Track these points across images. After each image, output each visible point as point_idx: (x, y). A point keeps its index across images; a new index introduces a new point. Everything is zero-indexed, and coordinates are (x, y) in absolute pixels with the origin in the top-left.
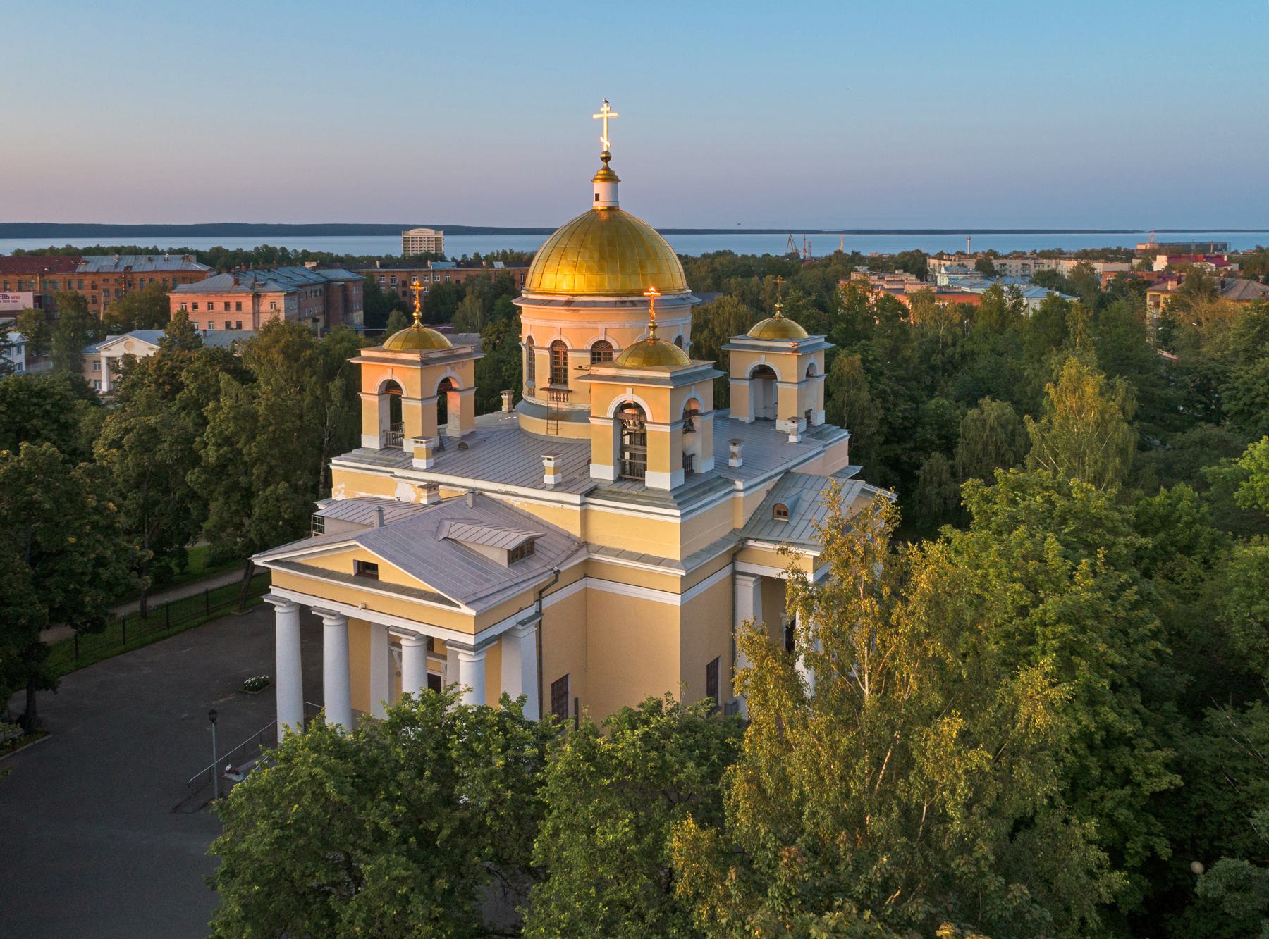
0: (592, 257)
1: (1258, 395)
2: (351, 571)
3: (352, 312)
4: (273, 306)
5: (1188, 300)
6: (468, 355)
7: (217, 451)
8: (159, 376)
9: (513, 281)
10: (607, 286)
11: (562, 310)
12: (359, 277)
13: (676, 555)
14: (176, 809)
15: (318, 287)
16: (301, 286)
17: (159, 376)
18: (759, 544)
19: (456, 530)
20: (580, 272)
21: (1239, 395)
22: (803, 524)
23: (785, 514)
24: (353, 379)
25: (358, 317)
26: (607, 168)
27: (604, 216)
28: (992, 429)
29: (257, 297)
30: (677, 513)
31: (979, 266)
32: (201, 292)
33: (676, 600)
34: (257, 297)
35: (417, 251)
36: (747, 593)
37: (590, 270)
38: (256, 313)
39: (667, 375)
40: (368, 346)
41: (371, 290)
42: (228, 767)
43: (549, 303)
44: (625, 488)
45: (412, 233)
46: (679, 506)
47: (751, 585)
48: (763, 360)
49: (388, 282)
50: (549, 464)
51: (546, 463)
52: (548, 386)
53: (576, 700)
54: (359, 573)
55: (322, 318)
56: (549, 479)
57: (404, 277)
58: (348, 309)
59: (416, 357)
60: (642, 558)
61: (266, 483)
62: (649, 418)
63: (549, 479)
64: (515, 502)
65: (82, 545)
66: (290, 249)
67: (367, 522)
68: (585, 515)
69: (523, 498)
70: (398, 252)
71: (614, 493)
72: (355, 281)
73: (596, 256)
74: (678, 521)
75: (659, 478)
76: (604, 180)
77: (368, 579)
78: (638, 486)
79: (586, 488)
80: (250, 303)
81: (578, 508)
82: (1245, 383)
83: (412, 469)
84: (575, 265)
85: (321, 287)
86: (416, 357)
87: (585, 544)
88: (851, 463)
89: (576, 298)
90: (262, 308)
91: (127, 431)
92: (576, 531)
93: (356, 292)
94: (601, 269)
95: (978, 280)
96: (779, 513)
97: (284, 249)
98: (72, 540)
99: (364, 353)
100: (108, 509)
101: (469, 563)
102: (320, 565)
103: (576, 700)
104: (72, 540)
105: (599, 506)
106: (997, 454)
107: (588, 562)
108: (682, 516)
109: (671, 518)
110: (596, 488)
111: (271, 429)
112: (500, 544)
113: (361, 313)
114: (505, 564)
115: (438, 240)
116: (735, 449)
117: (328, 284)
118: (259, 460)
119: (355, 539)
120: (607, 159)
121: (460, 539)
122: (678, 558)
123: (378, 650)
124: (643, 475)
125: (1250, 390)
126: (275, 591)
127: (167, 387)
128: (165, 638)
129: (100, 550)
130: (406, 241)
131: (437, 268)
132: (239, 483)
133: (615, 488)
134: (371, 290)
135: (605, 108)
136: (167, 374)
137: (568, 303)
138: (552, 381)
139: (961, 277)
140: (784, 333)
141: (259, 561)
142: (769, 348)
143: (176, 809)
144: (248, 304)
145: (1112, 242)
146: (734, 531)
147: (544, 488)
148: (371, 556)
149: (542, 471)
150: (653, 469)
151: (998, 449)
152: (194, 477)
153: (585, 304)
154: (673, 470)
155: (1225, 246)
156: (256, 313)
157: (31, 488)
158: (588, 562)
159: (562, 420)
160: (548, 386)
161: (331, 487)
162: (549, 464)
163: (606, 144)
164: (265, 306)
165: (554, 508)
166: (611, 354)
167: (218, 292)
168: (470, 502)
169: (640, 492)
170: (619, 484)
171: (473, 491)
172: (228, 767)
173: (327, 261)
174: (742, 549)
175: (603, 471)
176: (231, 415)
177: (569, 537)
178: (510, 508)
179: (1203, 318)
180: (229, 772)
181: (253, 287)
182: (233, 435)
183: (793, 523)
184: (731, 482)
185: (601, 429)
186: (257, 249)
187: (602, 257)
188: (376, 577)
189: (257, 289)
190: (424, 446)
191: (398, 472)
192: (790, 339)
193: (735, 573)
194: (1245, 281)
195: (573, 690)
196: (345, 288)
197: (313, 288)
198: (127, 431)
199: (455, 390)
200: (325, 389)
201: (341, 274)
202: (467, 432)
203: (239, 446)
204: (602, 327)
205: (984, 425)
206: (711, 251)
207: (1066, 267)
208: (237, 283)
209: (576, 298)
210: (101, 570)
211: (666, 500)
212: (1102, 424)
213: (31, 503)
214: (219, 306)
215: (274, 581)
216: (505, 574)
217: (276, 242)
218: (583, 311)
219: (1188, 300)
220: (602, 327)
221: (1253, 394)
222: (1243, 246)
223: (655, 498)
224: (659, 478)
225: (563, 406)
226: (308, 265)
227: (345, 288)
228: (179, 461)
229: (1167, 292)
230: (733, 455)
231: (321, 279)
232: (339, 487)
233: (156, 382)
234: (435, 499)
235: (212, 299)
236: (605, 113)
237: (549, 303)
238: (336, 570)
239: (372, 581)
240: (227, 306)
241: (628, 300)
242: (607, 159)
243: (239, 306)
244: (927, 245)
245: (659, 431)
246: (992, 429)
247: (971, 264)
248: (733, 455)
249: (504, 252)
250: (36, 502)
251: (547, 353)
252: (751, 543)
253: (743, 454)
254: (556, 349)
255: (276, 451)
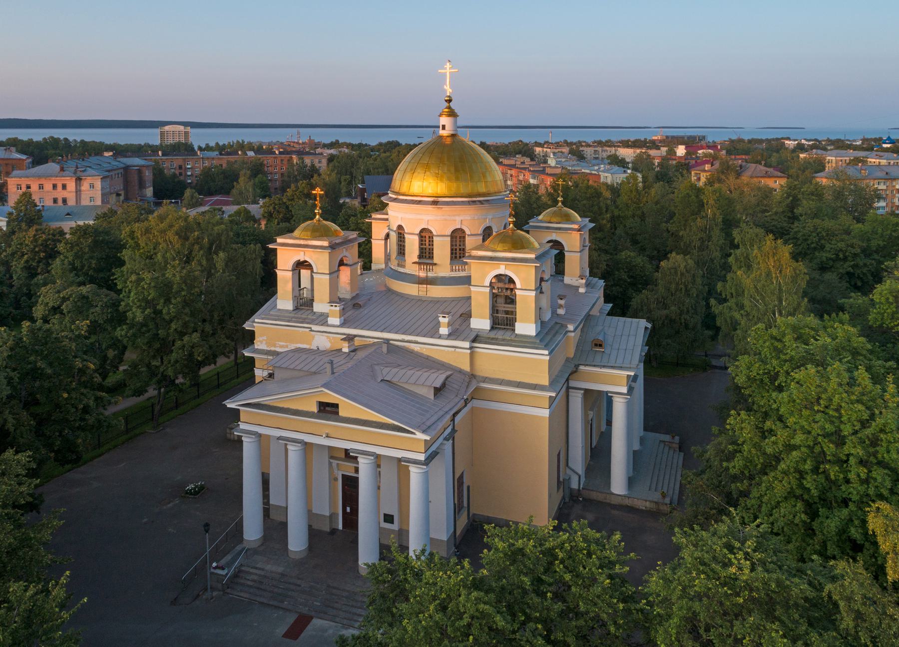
0: (449, 170)
1: (812, 243)
2: (315, 409)
3: (145, 188)
4: (92, 186)
5: (723, 177)
6: (355, 239)
7: (143, 312)
8: (35, 247)
9: (262, 164)
10: (462, 190)
11: (430, 208)
12: (150, 163)
13: (545, 382)
14: (174, 602)
15: (120, 171)
16: (109, 171)
17: (35, 247)
18: (587, 368)
19: (390, 373)
20: (441, 180)
21: (799, 242)
22: (614, 353)
23: (601, 345)
24: (269, 262)
25: (149, 192)
26: (449, 108)
27: (448, 141)
28: (682, 274)
29: (79, 180)
30: (546, 352)
31: (572, 152)
32: (33, 176)
33: (546, 413)
34: (79, 180)
35: (170, 141)
36: (577, 400)
37: (449, 179)
38: (78, 192)
39: (533, 256)
40: (281, 233)
41: (158, 172)
42: (214, 564)
43: (419, 202)
44: (499, 334)
45: (167, 128)
46: (546, 347)
47: (580, 396)
48: (554, 236)
49: (170, 165)
50: (444, 320)
51: (441, 319)
52: (417, 260)
53: (468, 487)
54: (320, 411)
55: (122, 193)
56: (444, 331)
57: (180, 163)
58: (142, 185)
59: (326, 244)
60: (520, 385)
61: (182, 334)
62: (518, 285)
63: (444, 331)
64: (416, 348)
65: (72, 398)
66: (71, 139)
67: (313, 370)
68: (472, 355)
69: (421, 344)
70: (157, 142)
71: (493, 339)
72: (147, 166)
73: (453, 169)
74: (548, 358)
75: (526, 327)
76: (449, 116)
77: (330, 415)
78: (509, 333)
79: (472, 337)
80: (74, 184)
81: (469, 351)
82: (804, 235)
83: (328, 325)
84: (437, 176)
85: (122, 170)
86: (326, 244)
87: (473, 376)
88: (605, 302)
89: (440, 199)
90: (83, 188)
91: (64, 299)
92: (466, 367)
93: (148, 175)
94: (457, 179)
95: (575, 163)
96: (596, 345)
97: (66, 139)
98: (65, 395)
99: (279, 240)
100: (89, 368)
101: (407, 398)
102: (281, 405)
103: (468, 487)
104: (65, 395)
105: (483, 349)
106: (686, 290)
107: (478, 389)
108: (550, 354)
109: (542, 356)
110: (477, 336)
111: (183, 293)
112: (428, 383)
113: (152, 188)
114: (432, 397)
115: (186, 133)
116: (562, 302)
117: (127, 169)
118: (176, 317)
119: (321, 386)
120: (449, 101)
121: (395, 380)
122: (547, 384)
123: (389, 475)
124: (514, 326)
125: (806, 240)
126: (242, 426)
127: (42, 255)
128: (100, 456)
129: (85, 401)
130: (162, 134)
131: (205, 156)
132: (158, 334)
133: (493, 335)
134: (158, 172)
135: (448, 65)
136: (42, 245)
137: (435, 203)
138: (420, 257)
139: (563, 160)
140: (567, 219)
141: (231, 404)
142: (560, 229)
143: (174, 602)
144: (71, 185)
145: (632, 136)
146: (568, 360)
147: (440, 337)
148: (332, 397)
149: (438, 324)
150: (521, 321)
151: (686, 286)
152: (123, 333)
153: (447, 203)
154: (536, 322)
155: (704, 137)
156: (78, 192)
157: (32, 358)
158: (478, 389)
159: (430, 284)
160: (417, 260)
161: (254, 339)
162: (444, 320)
163: (449, 90)
164: (85, 186)
165: (450, 351)
166: (464, 237)
167: (47, 176)
168: (385, 349)
169: (513, 337)
170: (495, 332)
171: (387, 341)
172: (214, 564)
173: (119, 151)
174: (575, 372)
175: (481, 323)
176: (153, 284)
177: (461, 371)
178: (412, 352)
179: (732, 188)
180: (215, 568)
181: (75, 173)
182: (153, 299)
183: (608, 351)
184: (564, 326)
185: (480, 296)
186: (45, 139)
187: (457, 170)
188: (337, 413)
189: (79, 174)
190: (338, 308)
191: (314, 328)
192: (573, 223)
193: (568, 388)
194: (754, 165)
195: (466, 482)
196: (140, 172)
197: (116, 172)
198: (64, 299)
199: (346, 265)
200: (210, 260)
201: (137, 161)
202: (354, 294)
203: (159, 307)
204: (458, 219)
205: (676, 273)
206: (384, 141)
207: (628, 154)
208: (62, 169)
209: (440, 199)
210: (87, 417)
211: (535, 343)
212: (794, 279)
213: (35, 369)
214: (48, 186)
215: (242, 418)
216: (434, 405)
217: (60, 134)
218: (446, 208)
219: (723, 177)
220: (458, 219)
221: (809, 242)
222: (719, 137)
223: (524, 342)
224: (526, 327)
225: (430, 274)
226: (106, 154)
227: (140, 172)
228: (110, 321)
229: (705, 171)
230: (561, 306)
231: (122, 166)
232: (261, 339)
233: (33, 251)
234: (352, 348)
235: (42, 181)
236: (448, 69)
237: (419, 202)
238: (300, 408)
239: (333, 416)
240: (55, 186)
241: (476, 199)
242: (449, 101)
243: (64, 187)
244: (528, 138)
245: (525, 296)
246: (682, 274)
247: (566, 150)
248: (561, 306)
249: (238, 142)
250: (40, 368)
251: (417, 238)
252: (582, 367)
253: (567, 307)
254: (423, 234)
255: (187, 310)
